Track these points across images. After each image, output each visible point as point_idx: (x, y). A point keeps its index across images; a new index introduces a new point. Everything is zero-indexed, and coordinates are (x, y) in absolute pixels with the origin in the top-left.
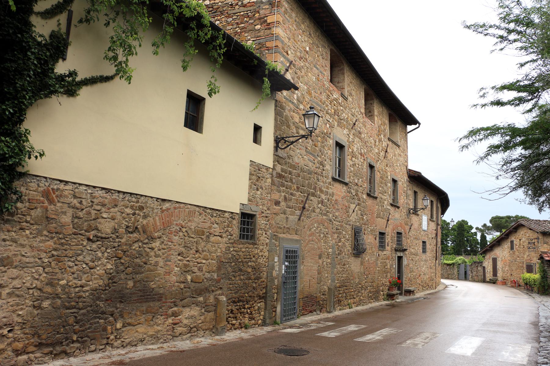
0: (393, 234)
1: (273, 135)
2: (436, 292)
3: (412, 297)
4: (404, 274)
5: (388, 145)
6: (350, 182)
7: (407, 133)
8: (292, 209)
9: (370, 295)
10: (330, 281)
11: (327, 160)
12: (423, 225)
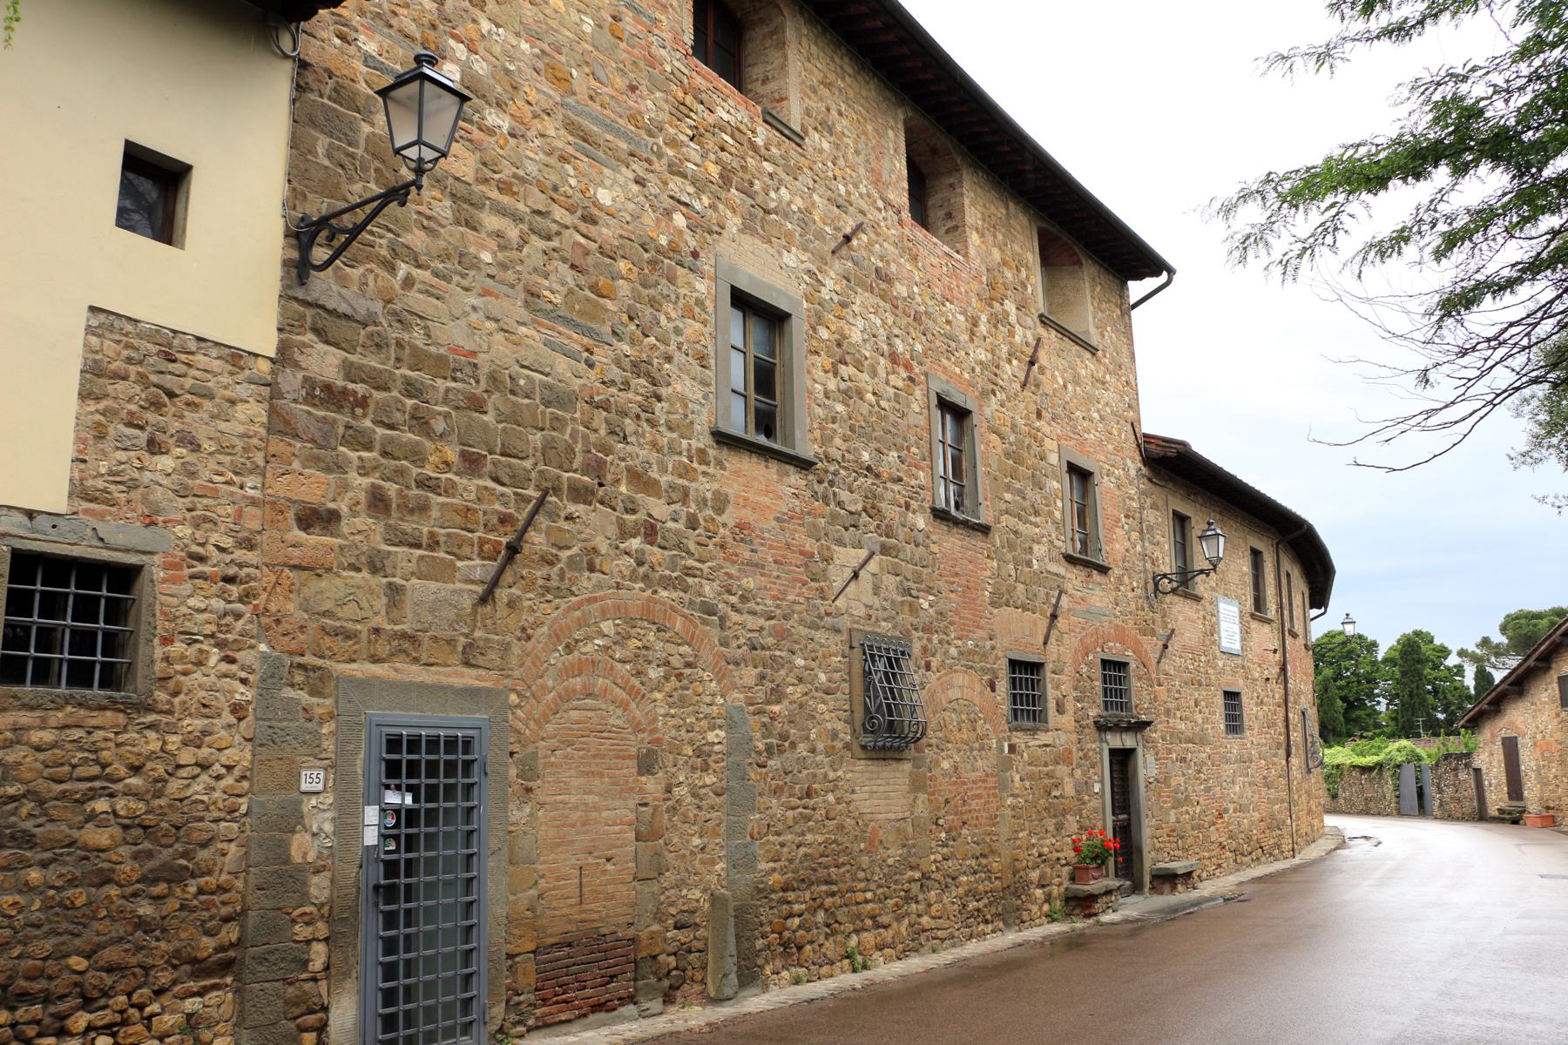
0: (1084, 669)
1: (277, 210)
2: (1296, 869)
3: (1182, 896)
4: (1144, 811)
5: (1039, 340)
6: (829, 459)
7: (1127, 309)
8: (430, 547)
9: (972, 905)
10: (720, 866)
11: (679, 357)
12: (1223, 634)
